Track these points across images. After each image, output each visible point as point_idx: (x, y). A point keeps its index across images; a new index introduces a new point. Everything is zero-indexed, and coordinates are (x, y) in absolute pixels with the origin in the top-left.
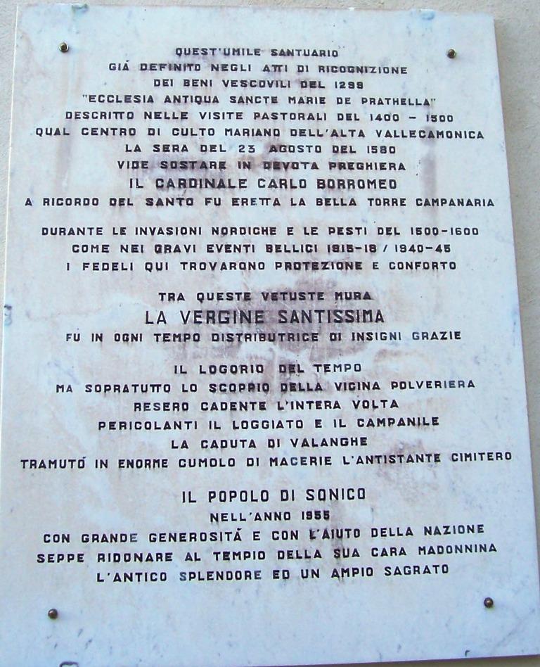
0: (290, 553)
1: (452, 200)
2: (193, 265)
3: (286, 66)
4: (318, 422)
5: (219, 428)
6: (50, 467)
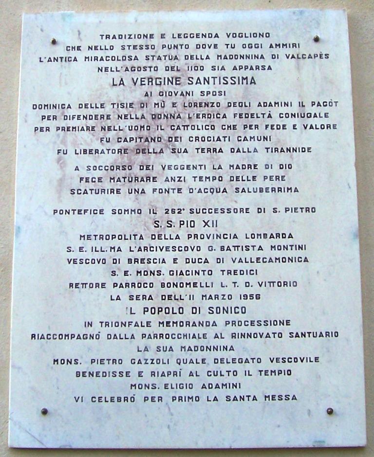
0: (237, 178)
1: (251, 67)
2: (197, 138)
3: (205, 166)
4: (175, 260)
5: (199, 376)
6: (275, 106)
